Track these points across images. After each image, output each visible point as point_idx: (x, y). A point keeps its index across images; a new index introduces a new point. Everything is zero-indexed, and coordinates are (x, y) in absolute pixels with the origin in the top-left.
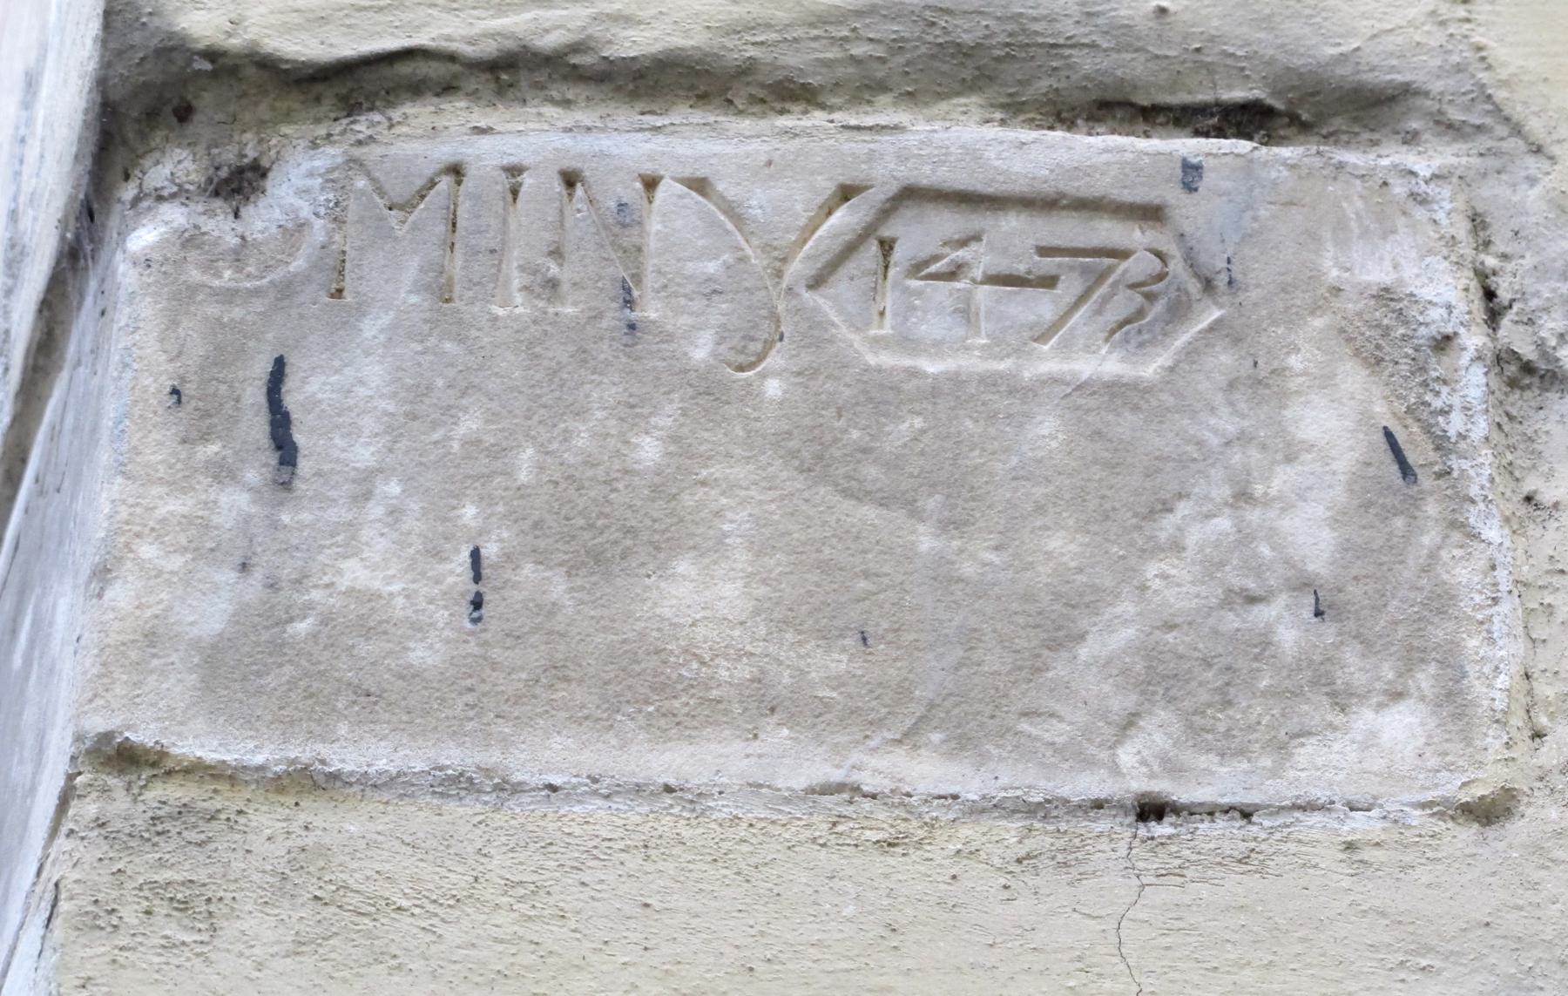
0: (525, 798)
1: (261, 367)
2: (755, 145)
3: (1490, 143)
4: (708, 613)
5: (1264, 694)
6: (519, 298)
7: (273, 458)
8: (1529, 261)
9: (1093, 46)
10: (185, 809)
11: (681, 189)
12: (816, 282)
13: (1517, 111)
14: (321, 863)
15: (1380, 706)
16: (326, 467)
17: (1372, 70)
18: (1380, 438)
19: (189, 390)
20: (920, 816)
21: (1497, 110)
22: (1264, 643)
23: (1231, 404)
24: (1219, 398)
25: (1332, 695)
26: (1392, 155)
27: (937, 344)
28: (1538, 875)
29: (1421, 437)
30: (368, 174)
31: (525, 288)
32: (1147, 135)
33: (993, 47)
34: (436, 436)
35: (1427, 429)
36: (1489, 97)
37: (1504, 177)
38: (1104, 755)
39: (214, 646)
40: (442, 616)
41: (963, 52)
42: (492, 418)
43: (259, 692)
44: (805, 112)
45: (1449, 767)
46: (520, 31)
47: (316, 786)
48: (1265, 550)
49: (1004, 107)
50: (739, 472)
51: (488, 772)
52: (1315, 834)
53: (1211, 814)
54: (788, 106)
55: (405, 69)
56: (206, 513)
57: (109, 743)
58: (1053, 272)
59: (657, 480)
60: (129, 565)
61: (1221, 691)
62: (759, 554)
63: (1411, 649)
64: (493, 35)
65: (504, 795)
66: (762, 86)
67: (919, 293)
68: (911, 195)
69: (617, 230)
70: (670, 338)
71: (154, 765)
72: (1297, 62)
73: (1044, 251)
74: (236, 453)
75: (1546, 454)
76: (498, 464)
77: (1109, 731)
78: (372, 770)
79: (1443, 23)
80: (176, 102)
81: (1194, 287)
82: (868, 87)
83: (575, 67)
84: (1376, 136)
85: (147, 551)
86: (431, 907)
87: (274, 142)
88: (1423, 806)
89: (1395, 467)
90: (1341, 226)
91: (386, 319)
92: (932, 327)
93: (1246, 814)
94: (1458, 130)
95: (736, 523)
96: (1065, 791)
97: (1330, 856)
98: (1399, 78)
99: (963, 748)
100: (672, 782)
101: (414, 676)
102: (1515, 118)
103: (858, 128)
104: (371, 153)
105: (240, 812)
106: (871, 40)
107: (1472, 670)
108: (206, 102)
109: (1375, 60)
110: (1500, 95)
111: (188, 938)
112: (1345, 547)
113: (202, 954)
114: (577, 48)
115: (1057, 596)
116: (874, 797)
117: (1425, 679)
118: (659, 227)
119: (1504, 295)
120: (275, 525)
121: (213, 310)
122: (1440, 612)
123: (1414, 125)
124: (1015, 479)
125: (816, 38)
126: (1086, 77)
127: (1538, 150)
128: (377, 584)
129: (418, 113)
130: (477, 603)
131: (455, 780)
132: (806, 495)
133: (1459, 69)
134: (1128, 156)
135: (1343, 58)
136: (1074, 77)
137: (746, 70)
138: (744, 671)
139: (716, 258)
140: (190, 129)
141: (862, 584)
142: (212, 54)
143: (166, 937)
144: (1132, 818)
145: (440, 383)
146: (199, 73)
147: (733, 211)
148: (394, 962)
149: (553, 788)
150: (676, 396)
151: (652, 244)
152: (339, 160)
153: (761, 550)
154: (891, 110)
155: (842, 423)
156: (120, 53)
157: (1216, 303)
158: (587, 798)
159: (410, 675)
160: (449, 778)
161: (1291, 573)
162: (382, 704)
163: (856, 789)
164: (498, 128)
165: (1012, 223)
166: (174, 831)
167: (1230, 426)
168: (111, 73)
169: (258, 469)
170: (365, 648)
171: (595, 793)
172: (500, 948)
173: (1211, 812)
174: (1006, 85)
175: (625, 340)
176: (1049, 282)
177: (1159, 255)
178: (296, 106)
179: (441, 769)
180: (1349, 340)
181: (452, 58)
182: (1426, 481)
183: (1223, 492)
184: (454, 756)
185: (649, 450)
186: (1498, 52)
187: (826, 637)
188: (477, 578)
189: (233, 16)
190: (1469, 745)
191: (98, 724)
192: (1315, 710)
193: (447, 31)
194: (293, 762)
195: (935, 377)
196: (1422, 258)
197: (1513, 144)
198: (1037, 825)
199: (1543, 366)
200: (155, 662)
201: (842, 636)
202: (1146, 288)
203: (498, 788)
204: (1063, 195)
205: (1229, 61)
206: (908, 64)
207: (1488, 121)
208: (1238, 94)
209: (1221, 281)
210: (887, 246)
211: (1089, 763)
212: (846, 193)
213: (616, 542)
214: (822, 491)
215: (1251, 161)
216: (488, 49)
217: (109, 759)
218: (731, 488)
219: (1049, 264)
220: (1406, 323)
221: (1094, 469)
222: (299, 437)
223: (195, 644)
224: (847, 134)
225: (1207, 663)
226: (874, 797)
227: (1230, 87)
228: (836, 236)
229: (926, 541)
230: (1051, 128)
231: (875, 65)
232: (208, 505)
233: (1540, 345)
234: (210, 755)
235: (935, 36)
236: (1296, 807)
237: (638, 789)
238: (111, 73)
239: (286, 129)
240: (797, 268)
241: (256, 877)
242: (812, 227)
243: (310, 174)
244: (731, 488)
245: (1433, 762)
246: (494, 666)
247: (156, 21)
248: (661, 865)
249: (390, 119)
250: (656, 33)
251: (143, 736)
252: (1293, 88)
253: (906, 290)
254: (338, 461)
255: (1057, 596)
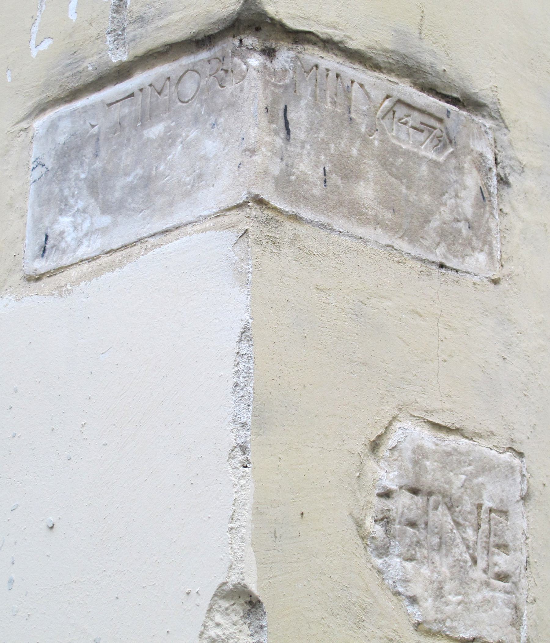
0: (335, 233)
1: (282, 107)
2: (371, 79)
3: (498, 123)
4: (367, 197)
5: (460, 244)
6: (329, 104)
7: (286, 132)
8: (504, 154)
9: (431, 74)
10: (272, 218)
11: (358, 86)
12: (383, 118)
13: (504, 117)
14: (299, 239)
15: (479, 252)
16: (296, 137)
17: (480, 98)
18: (479, 188)
19: (269, 108)
20: (404, 257)
21: (500, 115)
22: (460, 232)
23: (455, 172)
24: (453, 170)
25: (472, 247)
26: (479, 120)
27: (404, 141)
28: (505, 299)
29: (486, 191)
30: (300, 61)
31: (331, 102)
32: (440, 100)
33: (414, 68)
34: (316, 136)
35: (488, 189)
36: (499, 112)
37: (500, 132)
38: (434, 251)
39: (277, 178)
40: (319, 183)
41: (409, 68)
42: (326, 134)
43: (286, 192)
44: (379, 73)
45: (490, 270)
46: (331, 34)
47: (297, 219)
48: (460, 210)
49: (413, 83)
50: (371, 162)
51: (329, 225)
52: (468, 279)
53: (451, 269)
54: (376, 70)
55: (308, 36)
56: (274, 143)
57: (257, 197)
58: (423, 129)
59: (356, 160)
60: (260, 152)
61: (453, 241)
62: (375, 184)
63: (484, 241)
64: (326, 34)
65: (332, 231)
66: (372, 63)
67: (400, 127)
68: (400, 102)
69: (347, 92)
70: (357, 124)
71: (266, 205)
72: (467, 91)
73: (422, 123)
74: (279, 128)
75: (504, 200)
76: (327, 147)
77: (435, 245)
78: (308, 218)
79: (492, 91)
80: (257, 26)
81: (448, 141)
82: (391, 70)
83: (340, 47)
84: (477, 113)
85: (263, 149)
86: (320, 256)
87: (279, 45)
88: (487, 278)
89: (482, 197)
90: (473, 135)
91: (306, 102)
92: (403, 136)
93: (457, 271)
94: (493, 117)
95: (371, 175)
96: (428, 258)
97: (471, 285)
98: (484, 102)
99: (411, 243)
100: (362, 237)
101: (315, 197)
102: (504, 119)
103: (390, 81)
104: (301, 56)
105: (283, 222)
106: (393, 59)
107: (494, 248)
108: (265, 29)
109: (480, 96)
110: (501, 112)
111: (276, 251)
112: (474, 213)
113: (278, 256)
114: (341, 42)
115: (426, 210)
116: (396, 250)
117: (486, 248)
118: (355, 94)
119: (499, 160)
120: (287, 150)
121: (272, 88)
122: (489, 234)
123: (485, 114)
124: (419, 179)
125: (383, 55)
126: (429, 82)
127: (507, 128)
128: (306, 171)
129: (309, 48)
130: (325, 182)
131: (322, 225)
132: (383, 172)
133: (495, 103)
134: (438, 105)
135: (475, 93)
136: (427, 81)
137: (370, 59)
138: (373, 213)
139: (365, 106)
140: (258, 33)
141: (393, 197)
142: (272, 19)
143: (271, 250)
144: (438, 267)
145: (316, 122)
146: (267, 22)
147: (367, 94)
148: (314, 267)
149: (340, 232)
150: (359, 139)
151: (353, 98)
152: (294, 56)
153: (376, 184)
154: (394, 77)
155: (388, 156)
156: (248, 9)
157: (452, 146)
158: (346, 236)
159: (313, 196)
160: (322, 224)
161: (465, 217)
162: (309, 202)
163: (393, 247)
164: (325, 58)
165: (416, 114)
166: (271, 223)
167: (455, 178)
168: (243, 12)
169: (283, 135)
170: (305, 187)
171: (348, 235)
172: (333, 269)
173: (452, 269)
174: (414, 78)
175: (350, 122)
176: (422, 131)
177: (441, 131)
178: (285, 37)
179: (320, 221)
180: (475, 163)
181: (318, 37)
182: (487, 202)
183: (453, 194)
184: (324, 220)
185: (355, 152)
186: (502, 102)
187: (388, 208)
188: (325, 175)
189: (277, 10)
190: (494, 266)
191: (255, 191)
192: (469, 251)
193: (318, 29)
194: (293, 212)
195: (405, 149)
196: (487, 147)
197: (502, 124)
198: (423, 264)
199: (505, 180)
200: (266, 179)
201: (390, 209)
202: (439, 138)
203: (331, 229)
204: (426, 111)
205: (455, 87)
206: (399, 67)
207: (498, 117)
208: (455, 95)
209: (453, 141)
210: (394, 112)
211: (432, 252)
212: (388, 97)
213: (349, 174)
214: (386, 172)
215: (458, 114)
216: (324, 37)
217: (256, 200)
218: (370, 166)
219: (423, 127)
220: (485, 163)
221: (432, 181)
222: (290, 128)
223: (273, 176)
224: (389, 82)
225: (451, 234)
226: (396, 250)
227: (454, 93)
228: (386, 108)
229: (404, 191)
230: (421, 91)
231: (393, 66)
232: (274, 140)
233: (505, 175)
234: (278, 207)
235: (404, 62)
236: (466, 272)
237: (355, 237)
238: (243, 12)
239: (282, 43)
240: (379, 113)
241: (287, 239)
242: (381, 104)
243: (288, 57)
244: (370, 166)
245: (488, 268)
246: (329, 198)
247: (260, 6)
248: (360, 256)
249: (304, 48)
250: (356, 44)
251: (265, 198)
252: (465, 97)
253: (398, 125)
254: (298, 136)
255: (426, 210)
